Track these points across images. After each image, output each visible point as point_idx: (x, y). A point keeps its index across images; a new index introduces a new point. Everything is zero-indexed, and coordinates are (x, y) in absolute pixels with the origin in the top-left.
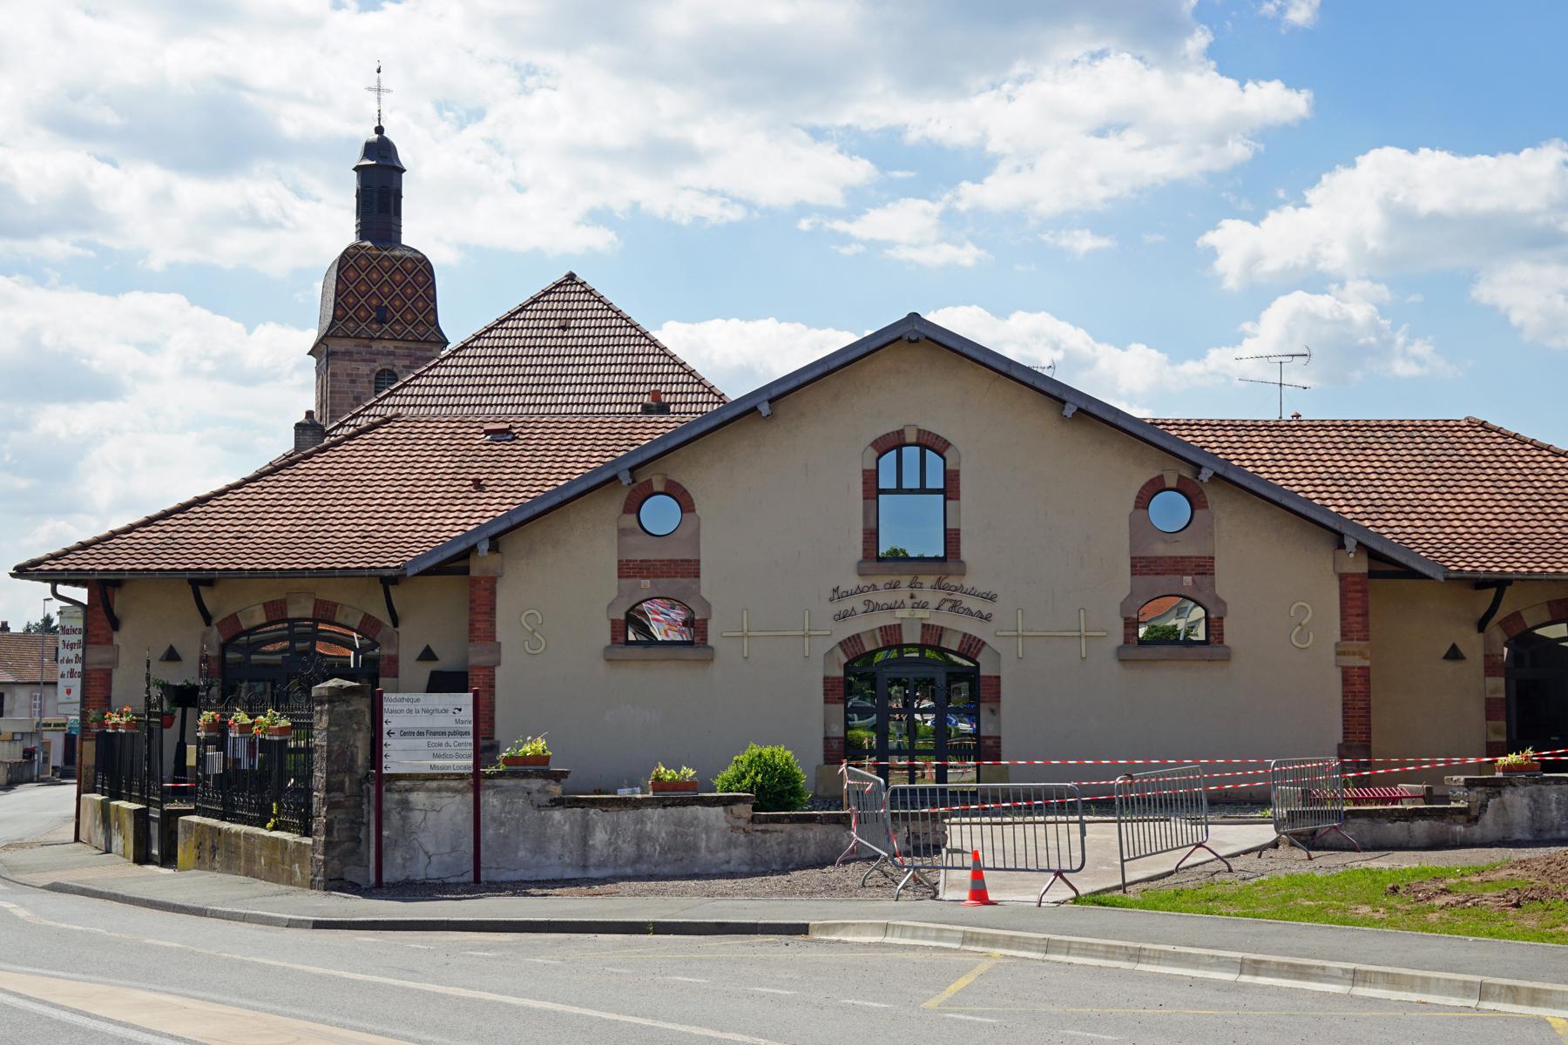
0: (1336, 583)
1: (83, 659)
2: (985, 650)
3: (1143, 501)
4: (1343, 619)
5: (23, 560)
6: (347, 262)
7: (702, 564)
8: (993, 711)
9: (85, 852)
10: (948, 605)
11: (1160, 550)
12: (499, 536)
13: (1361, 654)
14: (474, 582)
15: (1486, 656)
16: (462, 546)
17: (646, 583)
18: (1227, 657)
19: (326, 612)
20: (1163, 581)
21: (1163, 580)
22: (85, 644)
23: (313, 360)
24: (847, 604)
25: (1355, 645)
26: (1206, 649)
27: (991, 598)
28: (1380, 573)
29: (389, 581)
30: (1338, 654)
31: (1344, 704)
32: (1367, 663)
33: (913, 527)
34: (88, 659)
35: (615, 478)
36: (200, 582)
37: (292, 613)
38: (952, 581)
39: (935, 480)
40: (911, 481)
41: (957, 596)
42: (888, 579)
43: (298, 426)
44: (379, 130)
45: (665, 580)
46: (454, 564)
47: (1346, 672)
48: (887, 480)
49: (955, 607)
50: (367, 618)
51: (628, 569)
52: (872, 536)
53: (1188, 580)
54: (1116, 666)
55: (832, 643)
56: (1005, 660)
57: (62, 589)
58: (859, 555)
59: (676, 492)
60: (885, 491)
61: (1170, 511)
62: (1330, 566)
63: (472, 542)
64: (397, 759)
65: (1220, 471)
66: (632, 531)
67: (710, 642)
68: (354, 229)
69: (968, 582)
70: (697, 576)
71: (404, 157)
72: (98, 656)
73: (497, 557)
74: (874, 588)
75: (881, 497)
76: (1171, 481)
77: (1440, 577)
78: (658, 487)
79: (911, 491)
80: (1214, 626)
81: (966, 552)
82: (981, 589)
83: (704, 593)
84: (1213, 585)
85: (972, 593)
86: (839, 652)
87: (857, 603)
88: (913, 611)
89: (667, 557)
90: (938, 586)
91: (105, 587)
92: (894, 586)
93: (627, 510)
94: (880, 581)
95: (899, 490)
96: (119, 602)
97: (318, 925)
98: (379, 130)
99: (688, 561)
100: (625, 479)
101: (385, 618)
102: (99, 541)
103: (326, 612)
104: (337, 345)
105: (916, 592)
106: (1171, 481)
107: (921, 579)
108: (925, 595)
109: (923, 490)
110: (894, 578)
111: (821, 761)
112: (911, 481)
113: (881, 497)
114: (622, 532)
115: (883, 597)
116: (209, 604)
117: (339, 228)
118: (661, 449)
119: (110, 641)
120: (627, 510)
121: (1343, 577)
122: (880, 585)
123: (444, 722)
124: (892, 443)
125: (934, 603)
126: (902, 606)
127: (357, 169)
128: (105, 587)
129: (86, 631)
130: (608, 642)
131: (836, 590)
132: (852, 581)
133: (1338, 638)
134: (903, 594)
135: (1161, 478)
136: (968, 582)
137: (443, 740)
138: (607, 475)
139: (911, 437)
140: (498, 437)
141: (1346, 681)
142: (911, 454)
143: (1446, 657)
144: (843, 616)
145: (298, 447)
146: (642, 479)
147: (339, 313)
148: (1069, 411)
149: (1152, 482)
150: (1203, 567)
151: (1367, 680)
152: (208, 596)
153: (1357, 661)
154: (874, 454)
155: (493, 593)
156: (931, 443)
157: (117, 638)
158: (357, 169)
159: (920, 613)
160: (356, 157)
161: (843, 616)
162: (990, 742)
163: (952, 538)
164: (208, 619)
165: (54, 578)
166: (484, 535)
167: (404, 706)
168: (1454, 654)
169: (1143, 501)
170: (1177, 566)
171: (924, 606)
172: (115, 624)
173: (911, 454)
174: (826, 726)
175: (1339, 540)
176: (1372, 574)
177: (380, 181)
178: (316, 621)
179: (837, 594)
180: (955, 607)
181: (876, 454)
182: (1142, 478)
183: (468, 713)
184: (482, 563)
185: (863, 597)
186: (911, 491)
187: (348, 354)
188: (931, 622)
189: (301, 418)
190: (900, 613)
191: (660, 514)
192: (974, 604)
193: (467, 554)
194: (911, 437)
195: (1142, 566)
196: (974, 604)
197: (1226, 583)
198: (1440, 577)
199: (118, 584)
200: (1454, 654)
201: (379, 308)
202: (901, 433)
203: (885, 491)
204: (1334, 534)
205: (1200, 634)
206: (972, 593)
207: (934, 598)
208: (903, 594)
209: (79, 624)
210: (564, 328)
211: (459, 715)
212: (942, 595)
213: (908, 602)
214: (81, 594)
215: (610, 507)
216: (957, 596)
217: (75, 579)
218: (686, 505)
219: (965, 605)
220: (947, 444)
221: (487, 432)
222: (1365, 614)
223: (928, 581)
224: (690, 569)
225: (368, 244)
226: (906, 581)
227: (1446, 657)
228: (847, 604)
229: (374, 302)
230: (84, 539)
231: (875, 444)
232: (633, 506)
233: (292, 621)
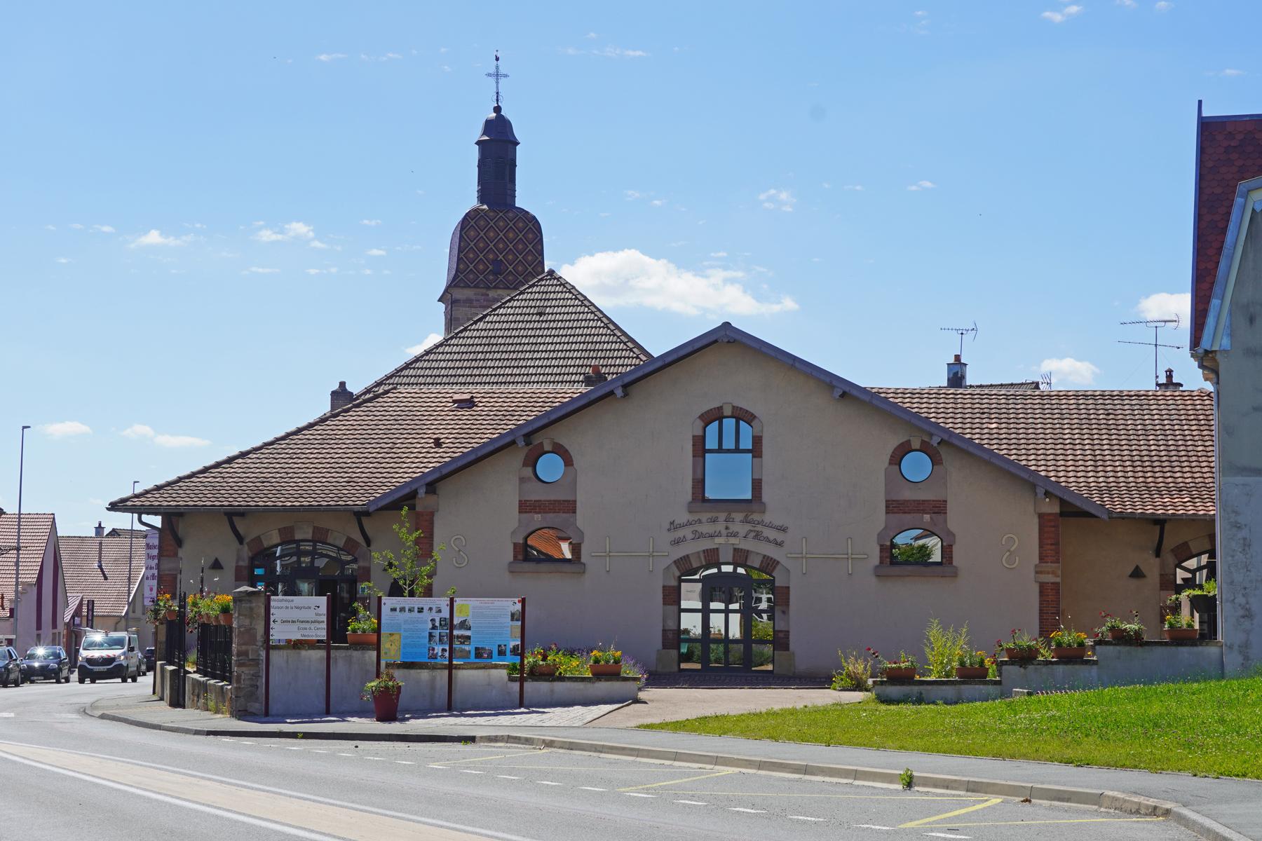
0: (1036, 520)
1: (158, 565)
2: (779, 567)
3: (897, 457)
4: (1041, 546)
5: (115, 498)
6: (469, 222)
7: (578, 504)
8: (784, 612)
9: (164, 705)
10: (753, 534)
11: (908, 494)
12: (433, 483)
13: (1053, 573)
14: (419, 515)
15: (1161, 575)
16: (407, 490)
17: (538, 517)
18: (955, 575)
19: (320, 536)
20: (908, 518)
21: (908, 516)
22: (160, 556)
23: (442, 306)
24: (680, 533)
25: (1050, 566)
26: (939, 568)
27: (783, 529)
28: (1067, 517)
29: (360, 515)
30: (1037, 572)
31: (1041, 611)
32: (1058, 580)
33: (728, 479)
34: (163, 567)
35: (513, 442)
36: (233, 516)
37: (298, 536)
38: (756, 517)
39: (746, 443)
40: (729, 443)
41: (759, 528)
42: (709, 515)
43: (333, 393)
44: (497, 109)
45: (551, 515)
46: (403, 500)
47: (1043, 587)
48: (711, 443)
49: (758, 536)
50: (349, 540)
51: (526, 507)
52: (699, 484)
53: (927, 517)
54: (874, 579)
55: (669, 561)
56: (793, 575)
57: (145, 518)
58: (689, 498)
59: (560, 450)
60: (711, 451)
61: (917, 466)
62: (1031, 508)
63: (414, 487)
64: (279, 633)
65: (946, 437)
66: (529, 479)
67: (583, 560)
68: (476, 194)
69: (767, 518)
70: (574, 512)
71: (518, 133)
72: (168, 565)
73: (432, 498)
74: (700, 521)
75: (707, 455)
76: (916, 444)
77: (1105, 517)
78: (547, 447)
79: (729, 451)
80: (947, 551)
81: (766, 496)
82: (778, 523)
83: (580, 523)
84: (945, 521)
85: (770, 526)
86: (674, 568)
87: (687, 532)
88: (729, 536)
89: (552, 498)
90: (746, 521)
91: (172, 517)
92: (714, 521)
93: (525, 464)
94: (705, 517)
95: (720, 450)
96: (181, 530)
97: (209, 733)
98: (497, 109)
99: (568, 501)
100: (521, 443)
101: (361, 540)
102: (169, 484)
103: (320, 536)
104: (461, 294)
105: (730, 525)
106: (916, 444)
107: (734, 515)
108: (734, 528)
109: (737, 450)
110: (714, 515)
111: (660, 646)
112: (729, 443)
113: (707, 455)
114: (522, 480)
115: (706, 528)
116: (241, 530)
117: (466, 196)
118: (545, 421)
119: (176, 554)
120: (525, 464)
121: (1041, 516)
122: (704, 520)
123: (310, 615)
124: (714, 416)
125: (742, 533)
126: (719, 535)
127: (478, 143)
128: (172, 517)
129: (160, 548)
130: (511, 559)
131: (672, 523)
132: (684, 517)
133: (1037, 561)
134: (720, 527)
135: (908, 442)
136: (767, 518)
137: (307, 626)
138: (508, 440)
139: (728, 411)
140: (463, 405)
141: (1042, 593)
142: (729, 424)
143: (1132, 576)
144: (677, 542)
145: (333, 408)
146: (536, 442)
147: (461, 266)
148: (838, 392)
149: (902, 444)
150: (939, 508)
151: (1058, 592)
152: (241, 526)
153: (1050, 578)
154: (700, 424)
155: (432, 523)
156: (742, 416)
157: (181, 553)
158: (478, 143)
159: (732, 540)
160: (477, 133)
161: (677, 542)
162: (781, 635)
163: (757, 485)
164: (240, 539)
165: (140, 511)
166: (422, 482)
167: (284, 604)
168: (1137, 574)
169: (897, 457)
170: (919, 507)
171: (735, 535)
172: (179, 543)
173: (729, 424)
174: (664, 621)
175: (1033, 487)
176: (1062, 514)
177: (498, 149)
178: (314, 541)
179: (673, 526)
180: (758, 536)
181: (702, 424)
182: (893, 442)
183: (323, 609)
184: (424, 501)
185: (692, 528)
186: (729, 451)
187: (469, 302)
188: (741, 547)
189: (336, 387)
190: (717, 540)
191: (550, 468)
192: (772, 534)
193: (412, 495)
194: (728, 411)
195: (893, 507)
196: (772, 534)
197: (954, 520)
198: (1105, 517)
199: (181, 515)
200: (1137, 574)
201: (496, 262)
202: (720, 408)
203: (711, 451)
204: (1025, 481)
205: (936, 557)
206: (770, 526)
207: (742, 529)
208: (720, 527)
209: (156, 542)
210: (540, 314)
211: (318, 611)
212: (748, 527)
213: (724, 532)
214: (157, 521)
215: (513, 462)
216: (759, 528)
217: (152, 511)
218: (568, 462)
219: (765, 535)
220: (753, 417)
221: (455, 402)
222: (1057, 544)
223: (739, 516)
224: (570, 507)
225: (485, 207)
226: (722, 516)
227: (1132, 576)
228: (680, 533)
229: (491, 256)
230: (158, 483)
231: (701, 417)
232: (532, 462)
233: (298, 542)
